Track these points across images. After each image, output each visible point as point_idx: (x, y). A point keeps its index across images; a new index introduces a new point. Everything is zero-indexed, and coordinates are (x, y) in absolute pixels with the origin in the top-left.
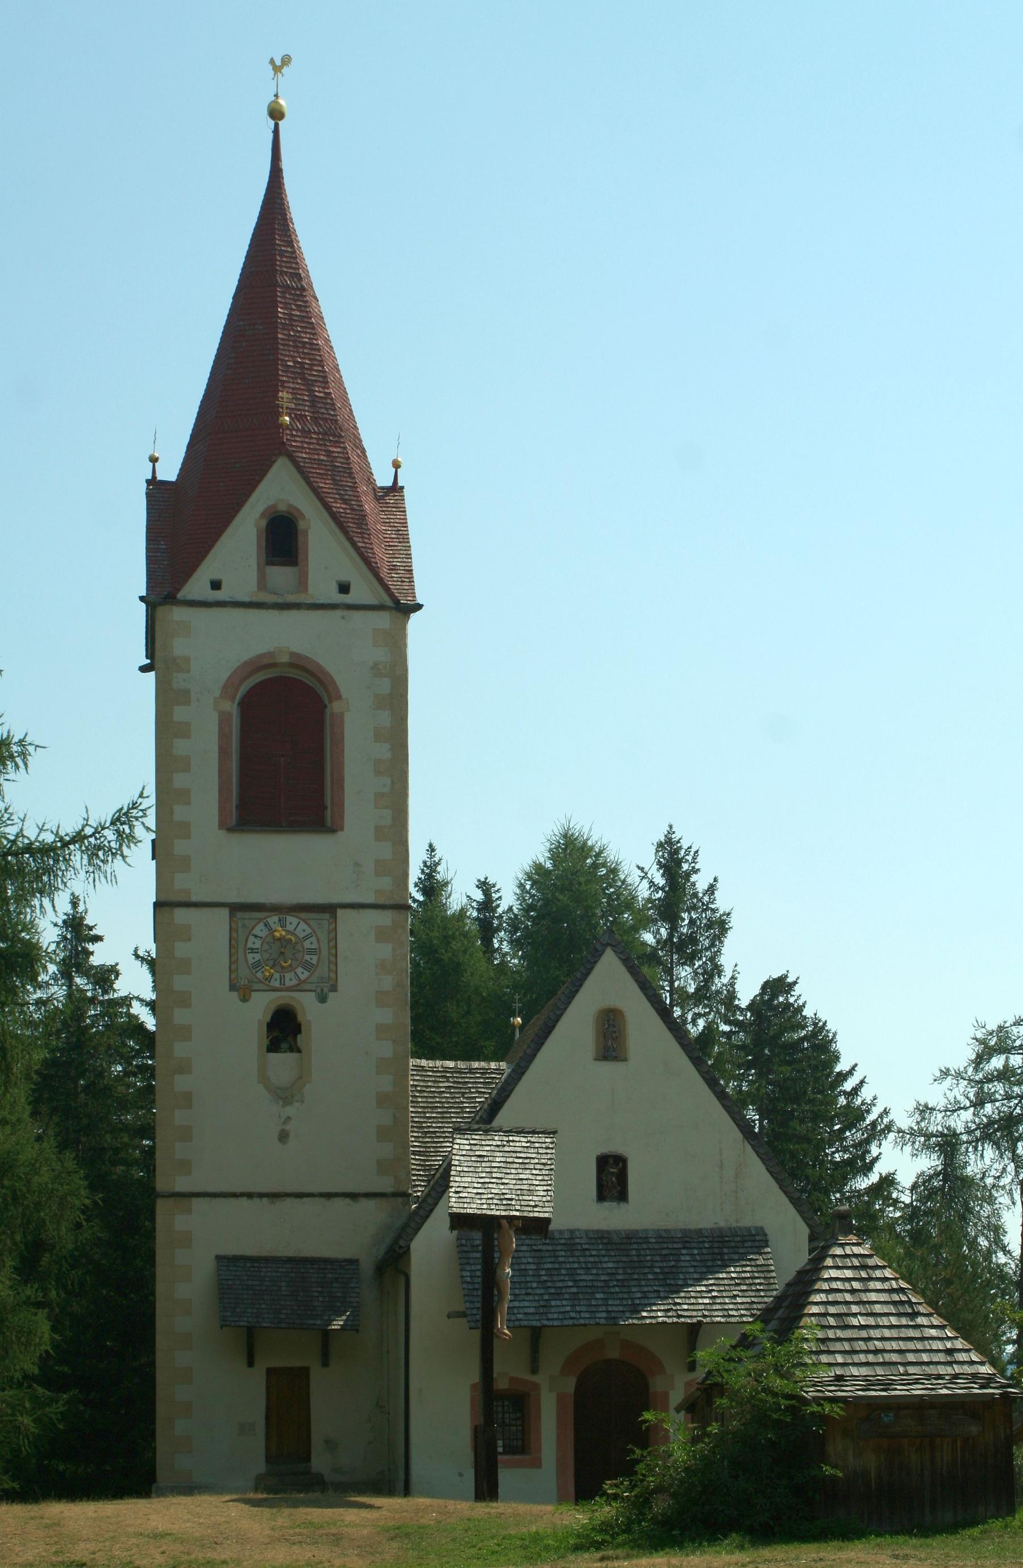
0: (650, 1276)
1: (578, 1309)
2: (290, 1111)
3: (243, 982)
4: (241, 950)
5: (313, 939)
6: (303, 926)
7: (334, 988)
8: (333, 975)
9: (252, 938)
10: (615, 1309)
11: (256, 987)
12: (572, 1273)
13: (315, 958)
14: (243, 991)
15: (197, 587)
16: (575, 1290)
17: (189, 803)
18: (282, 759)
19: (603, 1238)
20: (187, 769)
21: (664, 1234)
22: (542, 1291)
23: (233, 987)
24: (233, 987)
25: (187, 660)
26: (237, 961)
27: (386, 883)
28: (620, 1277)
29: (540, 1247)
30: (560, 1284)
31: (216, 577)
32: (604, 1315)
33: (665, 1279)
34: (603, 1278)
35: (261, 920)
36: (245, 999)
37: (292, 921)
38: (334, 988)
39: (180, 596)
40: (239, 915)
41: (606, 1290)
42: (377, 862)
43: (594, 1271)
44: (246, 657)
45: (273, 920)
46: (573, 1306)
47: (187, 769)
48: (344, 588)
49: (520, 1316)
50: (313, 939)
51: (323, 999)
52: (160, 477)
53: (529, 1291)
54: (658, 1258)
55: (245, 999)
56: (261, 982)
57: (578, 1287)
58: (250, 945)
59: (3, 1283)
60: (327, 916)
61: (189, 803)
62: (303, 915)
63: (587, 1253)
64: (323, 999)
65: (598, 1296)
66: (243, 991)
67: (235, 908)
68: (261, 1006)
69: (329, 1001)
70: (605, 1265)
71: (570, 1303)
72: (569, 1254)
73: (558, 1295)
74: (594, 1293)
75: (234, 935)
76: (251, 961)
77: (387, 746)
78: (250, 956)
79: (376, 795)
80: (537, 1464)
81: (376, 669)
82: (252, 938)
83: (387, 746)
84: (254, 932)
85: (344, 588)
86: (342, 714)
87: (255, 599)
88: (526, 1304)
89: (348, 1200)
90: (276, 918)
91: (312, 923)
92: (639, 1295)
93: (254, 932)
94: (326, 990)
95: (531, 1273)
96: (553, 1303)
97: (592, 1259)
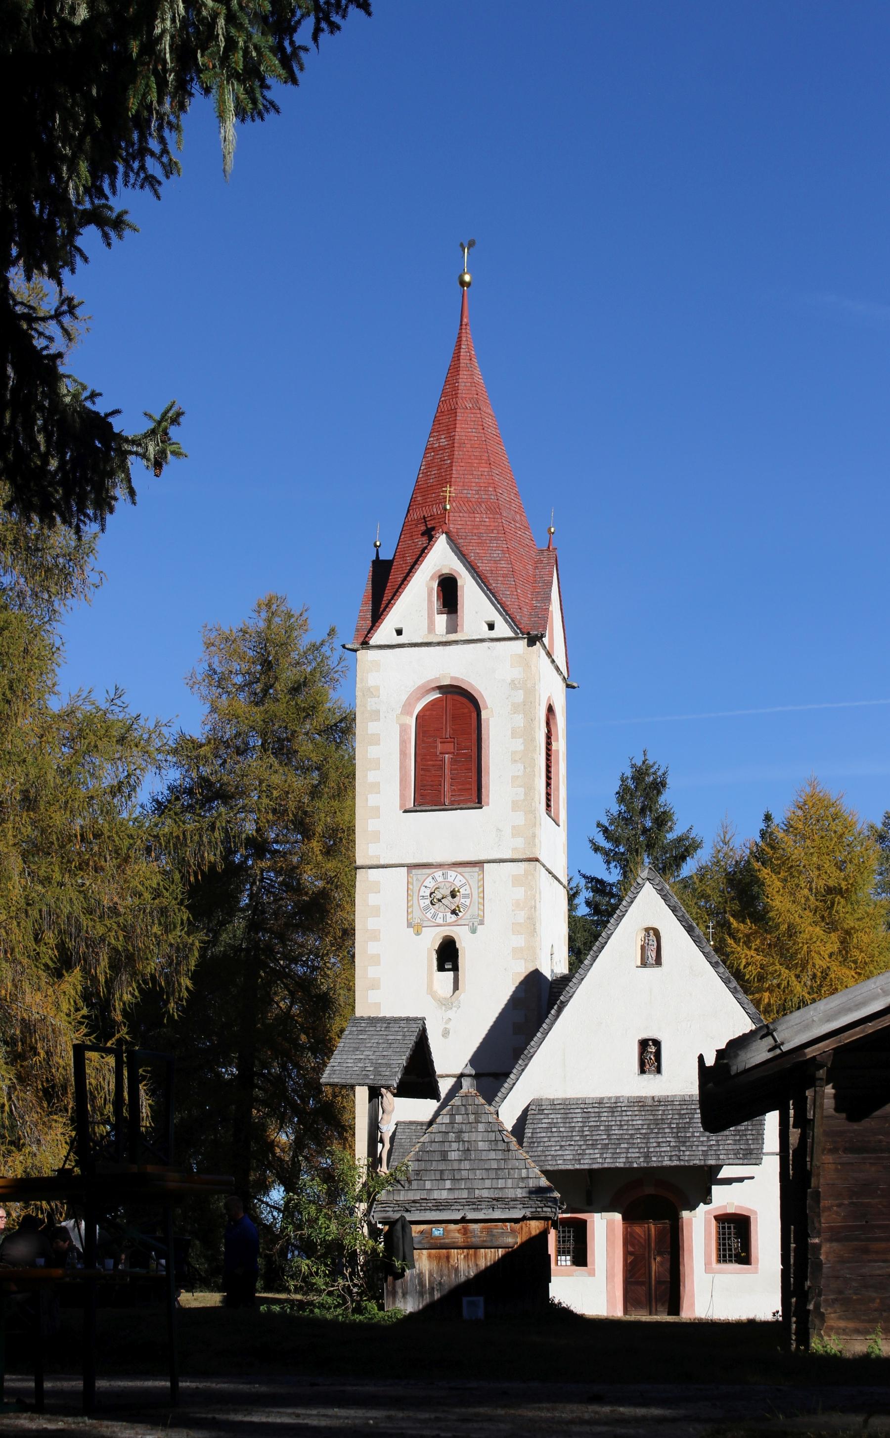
0: (667, 1130)
1: (605, 1156)
2: (450, 1014)
3: (417, 921)
4: (415, 898)
5: (467, 887)
6: (460, 877)
7: (482, 923)
8: (481, 913)
9: (423, 888)
10: (633, 1155)
11: (425, 924)
12: (608, 1128)
13: (468, 901)
14: (417, 928)
15: (384, 633)
16: (607, 1141)
17: (379, 793)
18: (447, 756)
19: (640, 1104)
20: (378, 768)
21: (687, 1098)
22: (582, 1143)
23: (409, 925)
24: (409, 925)
25: (377, 688)
26: (412, 906)
27: (519, 842)
28: (644, 1131)
29: (590, 1110)
30: (598, 1137)
31: (399, 626)
32: (624, 1160)
33: (677, 1133)
34: (630, 1132)
35: (430, 875)
36: (418, 933)
37: (452, 874)
38: (482, 923)
39: (372, 642)
40: (414, 871)
41: (631, 1141)
42: (513, 827)
43: (626, 1127)
44: (420, 682)
45: (438, 874)
46: (602, 1154)
47: (378, 768)
48: (491, 627)
49: (559, 1162)
50: (467, 887)
51: (474, 931)
52: (382, 557)
53: (573, 1143)
54: (677, 1117)
55: (418, 933)
56: (429, 920)
57: (610, 1139)
58: (422, 894)
59: (4, 1137)
60: (477, 869)
61: (379, 793)
62: (460, 869)
63: (624, 1113)
64: (474, 931)
65: (622, 1146)
66: (417, 928)
67: (412, 867)
68: (431, 940)
69: (478, 931)
70: (634, 1123)
71: (601, 1151)
72: (610, 1114)
73: (593, 1146)
74: (620, 1144)
75: (410, 886)
76: (422, 905)
77: (521, 740)
78: (422, 902)
79: (513, 777)
80: (592, 1274)
81: (513, 685)
82: (423, 888)
83: (521, 740)
84: (425, 884)
85: (491, 627)
86: (488, 719)
87: (426, 640)
88: (567, 1152)
89: (491, 1079)
90: (440, 873)
91: (466, 875)
92: (655, 1145)
93: (425, 884)
94: (476, 924)
95: (577, 1129)
96: (587, 1152)
97: (626, 1118)
